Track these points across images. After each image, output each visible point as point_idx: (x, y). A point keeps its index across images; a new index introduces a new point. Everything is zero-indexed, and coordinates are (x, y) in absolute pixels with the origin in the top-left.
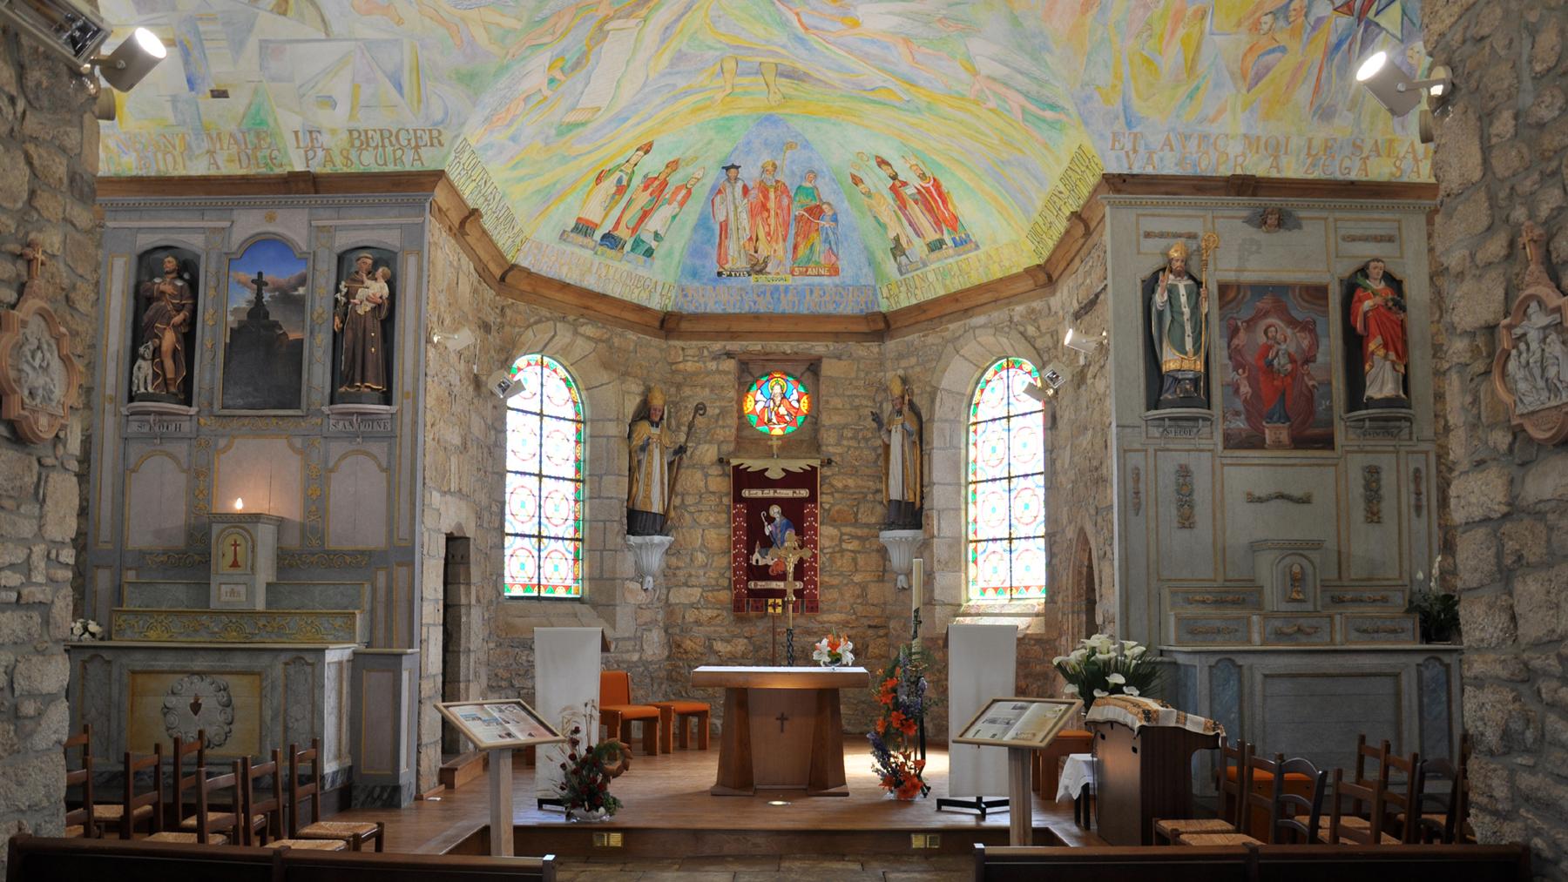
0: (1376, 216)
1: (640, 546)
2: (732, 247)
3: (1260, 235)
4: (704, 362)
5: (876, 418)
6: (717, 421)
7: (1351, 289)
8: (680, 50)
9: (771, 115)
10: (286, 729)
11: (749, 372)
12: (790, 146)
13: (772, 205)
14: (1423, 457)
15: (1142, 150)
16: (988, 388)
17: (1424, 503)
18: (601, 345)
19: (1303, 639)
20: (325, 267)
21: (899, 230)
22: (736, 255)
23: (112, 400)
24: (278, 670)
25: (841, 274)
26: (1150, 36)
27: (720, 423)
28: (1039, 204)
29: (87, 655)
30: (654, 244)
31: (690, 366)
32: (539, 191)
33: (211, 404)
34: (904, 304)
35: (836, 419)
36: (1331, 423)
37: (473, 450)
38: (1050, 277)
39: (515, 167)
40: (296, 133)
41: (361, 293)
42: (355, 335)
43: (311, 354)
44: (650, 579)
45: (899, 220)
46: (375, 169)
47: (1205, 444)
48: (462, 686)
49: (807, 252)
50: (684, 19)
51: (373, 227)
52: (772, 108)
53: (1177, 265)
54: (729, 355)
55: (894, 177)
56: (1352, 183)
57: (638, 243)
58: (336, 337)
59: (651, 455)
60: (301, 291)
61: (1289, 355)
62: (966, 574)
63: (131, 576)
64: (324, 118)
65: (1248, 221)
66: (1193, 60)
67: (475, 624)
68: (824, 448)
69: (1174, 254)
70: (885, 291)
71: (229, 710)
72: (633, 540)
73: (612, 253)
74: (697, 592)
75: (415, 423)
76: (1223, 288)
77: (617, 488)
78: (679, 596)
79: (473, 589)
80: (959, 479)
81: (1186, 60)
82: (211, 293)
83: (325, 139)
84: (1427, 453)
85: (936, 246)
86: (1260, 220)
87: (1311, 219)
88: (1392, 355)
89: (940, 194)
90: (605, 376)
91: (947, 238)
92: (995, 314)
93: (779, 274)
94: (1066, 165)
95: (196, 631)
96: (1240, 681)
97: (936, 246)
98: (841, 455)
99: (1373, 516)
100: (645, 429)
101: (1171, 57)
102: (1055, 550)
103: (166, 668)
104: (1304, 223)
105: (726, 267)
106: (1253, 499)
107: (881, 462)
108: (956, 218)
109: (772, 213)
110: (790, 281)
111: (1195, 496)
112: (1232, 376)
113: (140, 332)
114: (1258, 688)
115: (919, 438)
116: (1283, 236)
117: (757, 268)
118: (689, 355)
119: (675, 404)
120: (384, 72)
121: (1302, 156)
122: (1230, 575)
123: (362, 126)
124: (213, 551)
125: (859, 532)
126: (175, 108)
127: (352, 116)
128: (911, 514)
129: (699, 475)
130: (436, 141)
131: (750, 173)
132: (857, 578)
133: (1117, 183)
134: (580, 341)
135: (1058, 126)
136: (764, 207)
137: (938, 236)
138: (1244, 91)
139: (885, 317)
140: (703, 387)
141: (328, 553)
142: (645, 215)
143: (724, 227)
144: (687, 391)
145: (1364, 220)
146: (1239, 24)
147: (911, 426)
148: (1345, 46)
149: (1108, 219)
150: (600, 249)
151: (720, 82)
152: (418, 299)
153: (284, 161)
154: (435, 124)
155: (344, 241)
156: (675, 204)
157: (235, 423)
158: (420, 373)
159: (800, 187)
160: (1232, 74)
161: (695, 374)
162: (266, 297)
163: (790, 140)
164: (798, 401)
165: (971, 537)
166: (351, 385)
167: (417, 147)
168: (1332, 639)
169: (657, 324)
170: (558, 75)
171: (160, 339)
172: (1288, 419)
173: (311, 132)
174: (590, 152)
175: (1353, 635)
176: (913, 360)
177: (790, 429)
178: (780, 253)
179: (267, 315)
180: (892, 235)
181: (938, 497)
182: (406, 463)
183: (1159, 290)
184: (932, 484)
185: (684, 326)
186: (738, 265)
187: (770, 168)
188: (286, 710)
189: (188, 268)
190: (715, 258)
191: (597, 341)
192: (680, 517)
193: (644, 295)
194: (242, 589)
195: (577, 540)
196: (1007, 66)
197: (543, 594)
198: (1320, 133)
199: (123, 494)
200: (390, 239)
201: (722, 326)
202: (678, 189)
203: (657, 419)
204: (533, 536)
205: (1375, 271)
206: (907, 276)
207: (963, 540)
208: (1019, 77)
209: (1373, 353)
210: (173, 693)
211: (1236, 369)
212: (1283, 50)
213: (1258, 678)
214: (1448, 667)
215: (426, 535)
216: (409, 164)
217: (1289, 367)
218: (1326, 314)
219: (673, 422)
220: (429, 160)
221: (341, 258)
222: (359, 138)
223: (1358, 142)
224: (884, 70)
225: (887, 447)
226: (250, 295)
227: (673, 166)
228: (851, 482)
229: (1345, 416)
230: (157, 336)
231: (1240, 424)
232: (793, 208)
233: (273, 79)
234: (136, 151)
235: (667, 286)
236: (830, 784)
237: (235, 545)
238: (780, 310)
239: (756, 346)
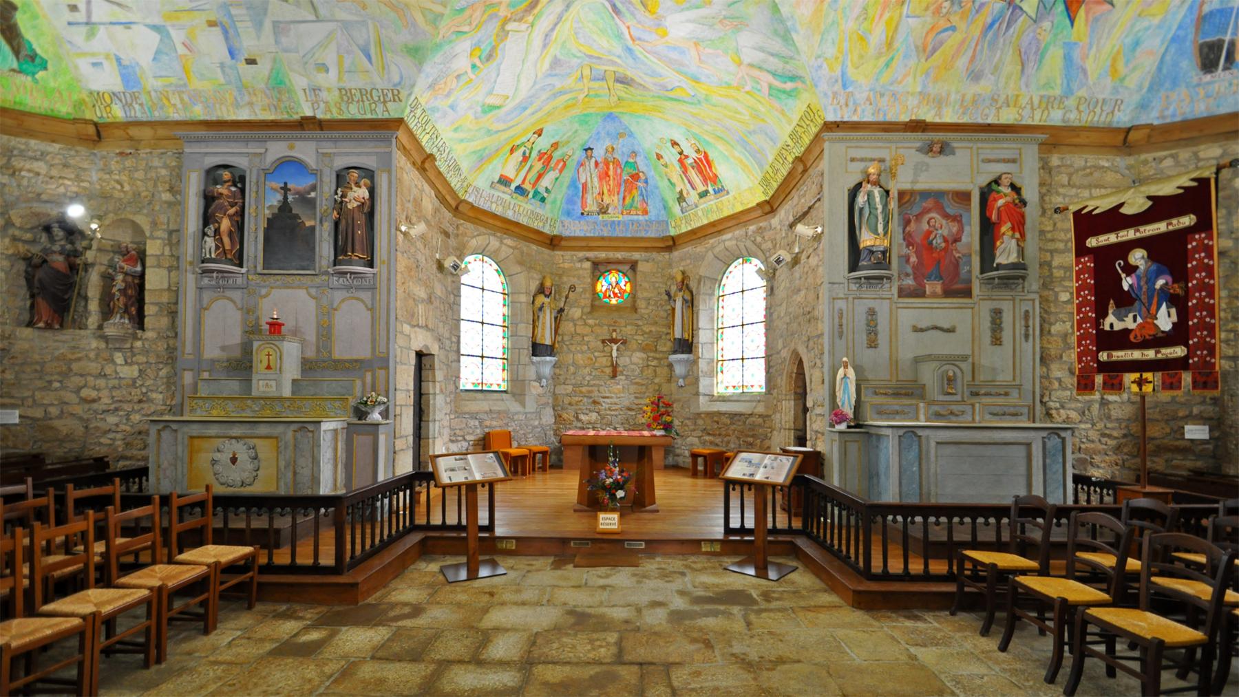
0: (1005, 146)
1: (539, 363)
2: (589, 198)
3: (926, 159)
5: (668, 294)
7: (986, 194)
8: (555, 56)
9: (611, 114)
10: (295, 474)
11: (599, 269)
12: (621, 135)
13: (611, 173)
14: (1031, 302)
15: (851, 104)
16: (730, 276)
17: (1031, 332)
18: (516, 251)
19: (954, 418)
20: (328, 180)
21: (682, 187)
23: (191, 263)
24: (290, 434)
26: (865, 19)
28: (771, 158)
29: (160, 426)
30: (545, 195)
31: (566, 265)
32: (474, 152)
33: (256, 267)
34: (684, 230)
35: (645, 294)
36: (970, 281)
37: (437, 303)
38: (772, 207)
39: (456, 130)
40: (304, 90)
41: (351, 195)
42: (347, 222)
43: (321, 235)
44: (544, 380)
46: (359, 117)
47: (886, 294)
48: (431, 441)
50: (558, 28)
51: (359, 154)
52: (611, 108)
53: (873, 178)
54: (588, 259)
55: (681, 153)
56: (989, 125)
57: (536, 193)
58: (337, 224)
59: (545, 313)
60: (313, 195)
61: (944, 237)
63: (206, 375)
64: (321, 79)
65: (919, 150)
66: (892, 37)
67: (439, 406)
69: (871, 170)
70: (673, 224)
71: (256, 461)
72: (535, 359)
73: (520, 198)
74: (570, 388)
75: (389, 280)
76: (901, 194)
77: (525, 331)
78: (561, 390)
79: (438, 385)
81: (887, 37)
82: (253, 195)
83: (324, 95)
84: (1033, 300)
85: (703, 195)
86: (928, 149)
87: (962, 148)
88: (1017, 235)
89: (708, 162)
90: (518, 269)
92: (737, 232)
93: (614, 215)
94: (794, 124)
95: (243, 410)
96: (920, 446)
97: (703, 195)
99: (997, 341)
100: (541, 299)
101: (878, 35)
102: (771, 364)
103: (213, 434)
104: (957, 150)
106: (916, 329)
107: (670, 318)
108: (716, 176)
110: (621, 218)
111: (879, 328)
112: (905, 251)
113: (207, 219)
114: (933, 451)
115: (691, 304)
116: (942, 159)
118: (563, 259)
119: (559, 286)
120: (358, 46)
121: (957, 107)
122: (901, 378)
123: (348, 85)
124: (254, 358)
125: (658, 356)
126: (223, 72)
127: (340, 79)
128: (686, 346)
129: (571, 324)
130: (397, 98)
131: (599, 153)
132: (657, 381)
133: (830, 127)
134: (504, 248)
135: (794, 94)
136: (607, 174)
138: (923, 60)
139: (673, 238)
141: (334, 361)
142: (540, 176)
143: (585, 186)
144: (565, 279)
145: (997, 148)
146: (927, 9)
147: (688, 297)
148: (996, 26)
149: (826, 153)
150: (515, 195)
151: (580, 86)
152: (389, 201)
153: (299, 110)
154: (395, 85)
155: (340, 163)
156: (557, 171)
157: (272, 279)
158: (392, 248)
159: (627, 162)
160: (917, 47)
162: (290, 198)
165: (720, 358)
166: (346, 255)
167: (385, 102)
168: (973, 419)
169: (549, 242)
170: (478, 63)
171: (219, 223)
172: (941, 278)
173: (314, 90)
174: (504, 130)
175: (988, 417)
176: (688, 261)
177: (621, 300)
178: (616, 201)
179: (291, 210)
180: (678, 190)
181: (703, 336)
182: (384, 304)
183: (862, 194)
185: (563, 243)
188: (295, 462)
189: (239, 180)
190: (580, 204)
191: (514, 248)
192: (561, 347)
193: (541, 224)
194: (273, 383)
196: (763, 51)
197: (485, 388)
198: (973, 89)
199: (200, 323)
200: (370, 162)
201: (584, 244)
202: (558, 161)
205: (1005, 181)
208: (771, 59)
209: (1004, 234)
210: (219, 451)
211: (908, 246)
212: (953, 29)
213: (933, 444)
214: (1064, 439)
215: (399, 350)
216: (380, 114)
217: (943, 245)
218: (969, 210)
220: (393, 112)
221: (339, 177)
222: (346, 95)
223: (996, 97)
224: (679, 72)
225: (674, 309)
226: (280, 197)
227: (555, 146)
228: (653, 329)
229: (980, 276)
230: (217, 222)
231: (910, 282)
232: (623, 175)
233: (286, 51)
234: (202, 102)
236: (647, 503)
237: (269, 355)
239: (602, 255)
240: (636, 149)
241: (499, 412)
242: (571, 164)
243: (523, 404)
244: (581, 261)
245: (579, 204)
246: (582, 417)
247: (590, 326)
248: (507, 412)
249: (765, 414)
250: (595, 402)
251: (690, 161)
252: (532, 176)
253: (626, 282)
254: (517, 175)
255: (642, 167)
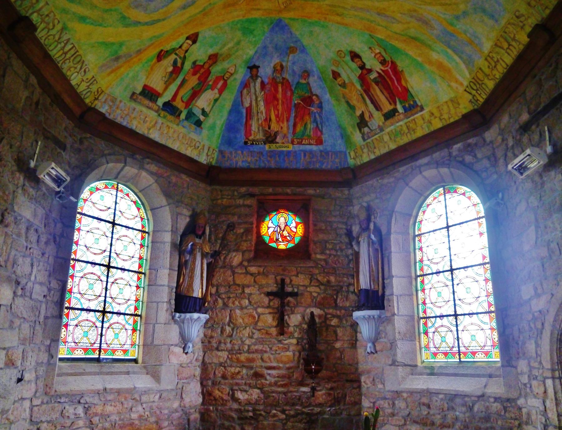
2: (254, 126)
4: (235, 200)
6: (242, 238)
12: (292, 50)
13: (280, 96)
22: (257, 130)
25: (324, 144)
27: (244, 238)
28: (487, 46)
30: (202, 118)
45: (363, 98)
49: (302, 128)
52: (280, 11)
54: (252, 195)
55: (362, 67)
57: (190, 115)
62: (419, 342)
68: (313, 256)
70: (352, 154)
80: (410, 272)
85: (390, 115)
91: (399, 108)
98: (325, 260)
105: (251, 138)
108: (406, 90)
109: (280, 101)
110: (291, 148)
117: (270, 139)
129: (229, 272)
131: (266, 71)
137: (391, 107)
140: (233, 215)
142: (195, 94)
143: (249, 110)
150: (163, 113)
156: (216, 91)
159: (298, 83)
161: (230, 207)
163: (292, 45)
164: (296, 228)
174: (147, 24)
177: (290, 245)
178: (285, 129)
180: (358, 113)
184: (391, 277)
186: (258, 137)
187: (279, 68)
195: (136, 315)
202: (218, 79)
203: (200, 233)
204: (98, 311)
206: (369, 140)
207: (416, 317)
219: (213, 238)
225: (357, 255)
227: (214, 58)
232: (294, 98)
235: (211, 150)
238: (285, 166)
240: (309, 66)
241: (119, 392)
242: (234, 84)
243: (156, 377)
244: (243, 196)
245: (243, 132)
246: (240, 396)
247: (252, 275)
248: (130, 391)
249: (505, 396)
250: (257, 375)
251: (373, 76)
252: (185, 93)
253: (297, 224)
254: (166, 89)
255: (316, 90)
